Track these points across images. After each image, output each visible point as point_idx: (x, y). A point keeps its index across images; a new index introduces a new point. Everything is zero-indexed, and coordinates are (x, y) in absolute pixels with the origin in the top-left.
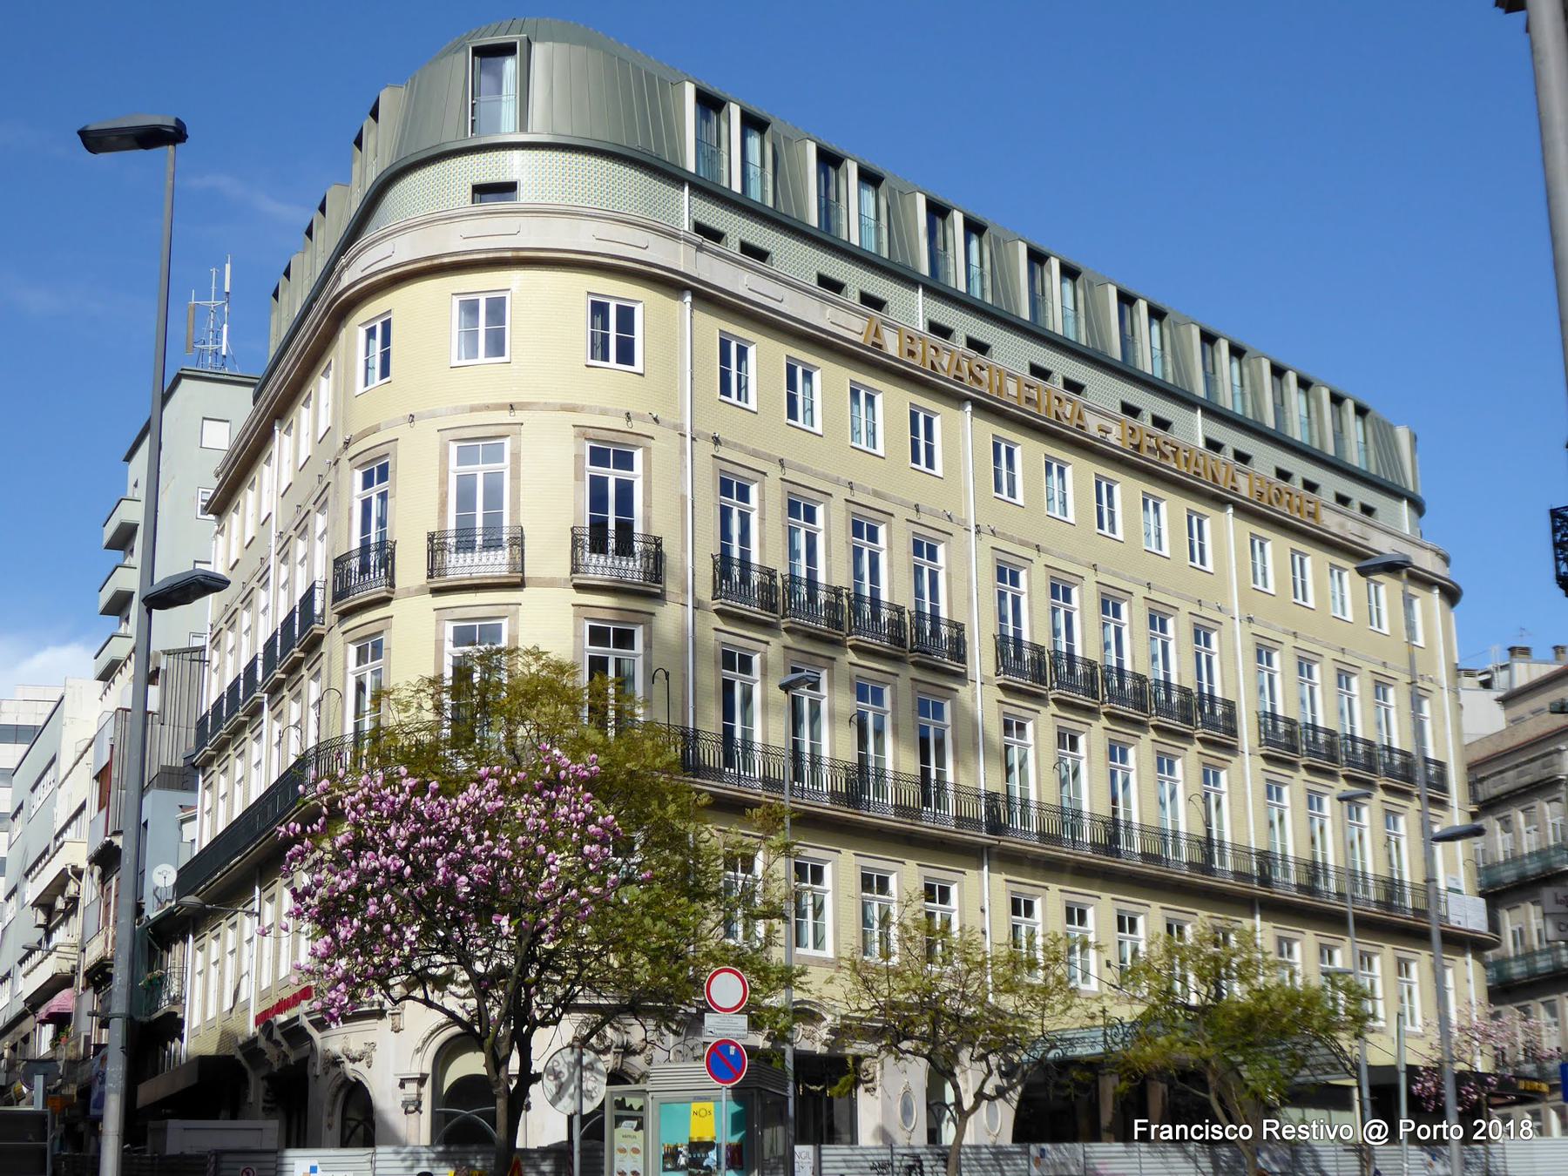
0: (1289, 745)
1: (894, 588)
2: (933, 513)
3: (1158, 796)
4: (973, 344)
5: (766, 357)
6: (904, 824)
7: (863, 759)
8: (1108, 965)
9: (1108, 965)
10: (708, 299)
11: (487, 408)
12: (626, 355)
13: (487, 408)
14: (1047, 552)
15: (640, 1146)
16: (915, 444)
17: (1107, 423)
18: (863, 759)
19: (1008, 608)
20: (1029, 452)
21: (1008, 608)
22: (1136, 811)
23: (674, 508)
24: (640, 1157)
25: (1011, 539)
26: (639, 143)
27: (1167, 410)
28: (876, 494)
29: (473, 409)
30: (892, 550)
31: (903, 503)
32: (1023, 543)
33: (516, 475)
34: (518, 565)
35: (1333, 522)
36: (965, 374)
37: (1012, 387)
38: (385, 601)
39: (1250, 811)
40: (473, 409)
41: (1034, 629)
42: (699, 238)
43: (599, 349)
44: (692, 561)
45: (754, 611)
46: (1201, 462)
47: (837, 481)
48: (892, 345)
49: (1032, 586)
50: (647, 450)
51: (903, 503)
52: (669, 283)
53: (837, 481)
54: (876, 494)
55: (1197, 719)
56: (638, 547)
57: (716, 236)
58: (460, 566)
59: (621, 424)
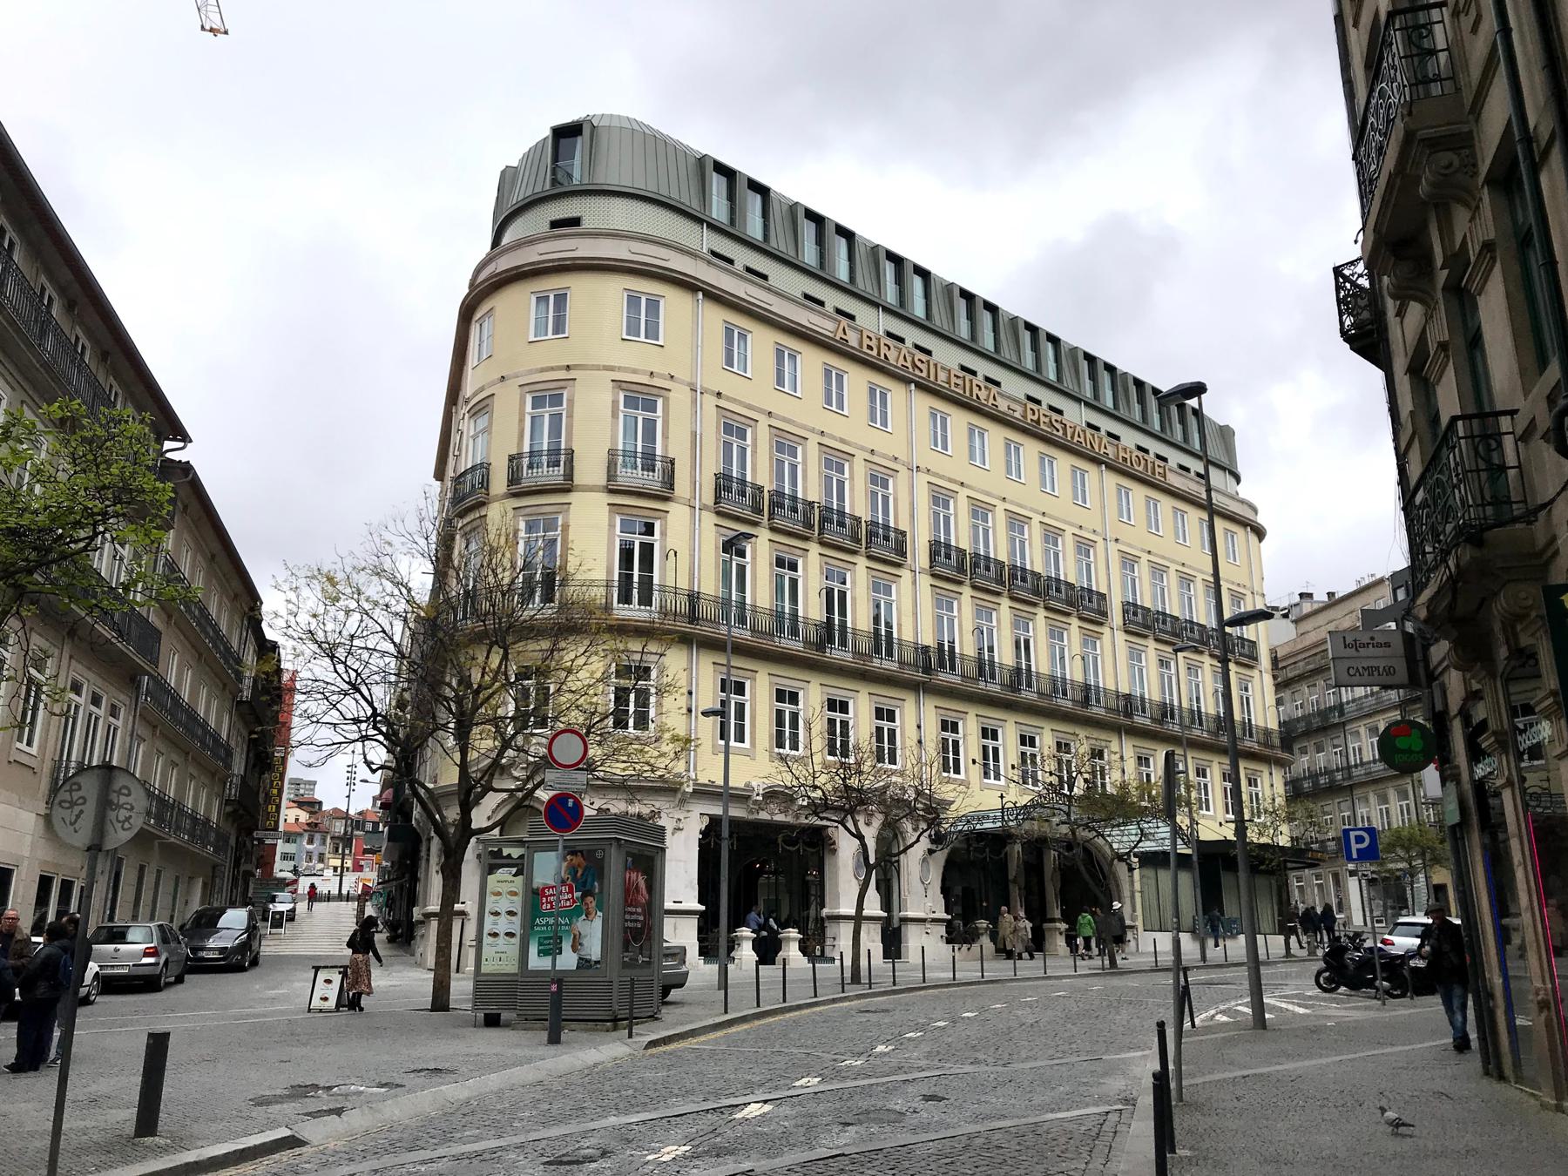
0: (955, 567)
1: (857, 504)
2: (884, 456)
3: (1058, 652)
4: (1158, 457)
5: (762, 342)
6: (1044, 703)
7: (830, 620)
8: (974, 762)
9: (974, 762)
10: (715, 297)
11: (552, 369)
12: (652, 332)
13: (552, 369)
14: (968, 487)
15: (489, 919)
16: (1149, 517)
17: (1013, 406)
18: (830, 620)
19: (941, 520)
20: (959, 420)
21: (941, 520)
22: (1041, 662)
23: (689, 438)
24: (487, 928)
25: (834, 438)
26: (652, 187)
27: (1116, 428)
28: (843, 441)
29: (542, 370)
30: (810, 462)
31: (862, 449)
32: (951, 480)
33: (570, 416)
34: (569, 475)
35: (1175, 480)
36: (909, 364)
37: (942, 376)
38: (483, 504)
39: (1119, 666)
40: (542, 370)
41: (962, 539)
42: (710, 257)
43: (633, 329)
44: (696, 478)
45: (799, 528)
46: (909, 359)
47: (813, 430)
48: (853, 339)
49: (960, 510)
50: (666, 400)
51: (862, 449)
52: (688, 285)
53: (813, 430)
54: (843, 441)
55: (1084, 605)
56: (659, 465)
57: (1187, 470)
58: (529, 478)
59: (645, 380)
